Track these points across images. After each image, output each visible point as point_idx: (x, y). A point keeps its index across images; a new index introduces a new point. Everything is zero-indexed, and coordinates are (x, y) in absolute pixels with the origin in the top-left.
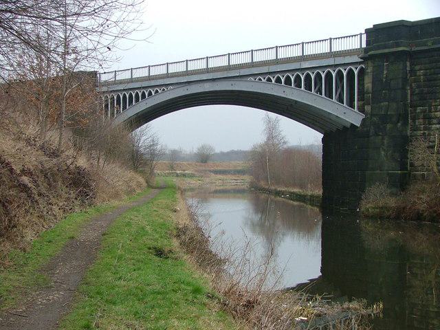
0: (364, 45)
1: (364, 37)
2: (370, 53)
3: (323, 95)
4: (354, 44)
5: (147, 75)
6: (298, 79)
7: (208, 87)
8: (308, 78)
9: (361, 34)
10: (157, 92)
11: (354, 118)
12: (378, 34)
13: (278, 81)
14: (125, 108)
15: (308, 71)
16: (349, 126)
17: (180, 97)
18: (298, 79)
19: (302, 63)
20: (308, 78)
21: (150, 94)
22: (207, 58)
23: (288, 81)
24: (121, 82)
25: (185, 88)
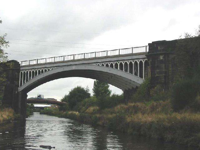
0: (148, 51)
1: (148, 48)
2: (150, 54)
3: (128, 72)
4: (143, 50)
5: (94, 57)
6: (116, 65)
7: (74, 68)
8: (121, 64)
9: (146, 46)
10: (49, 70)
11: (140, 81)
12: (154, 46)
13: (107, 66)
14: (33, 77)
15: (126, 61)
16: (135, 87)
17: (62, 72)
18: (116, 65)
19: (68, 63)
20: (121, 64)
21: (46, 71)
22: (132, 48)
23: (112, 66)
24: (89, 59)
25: (63, 68)
